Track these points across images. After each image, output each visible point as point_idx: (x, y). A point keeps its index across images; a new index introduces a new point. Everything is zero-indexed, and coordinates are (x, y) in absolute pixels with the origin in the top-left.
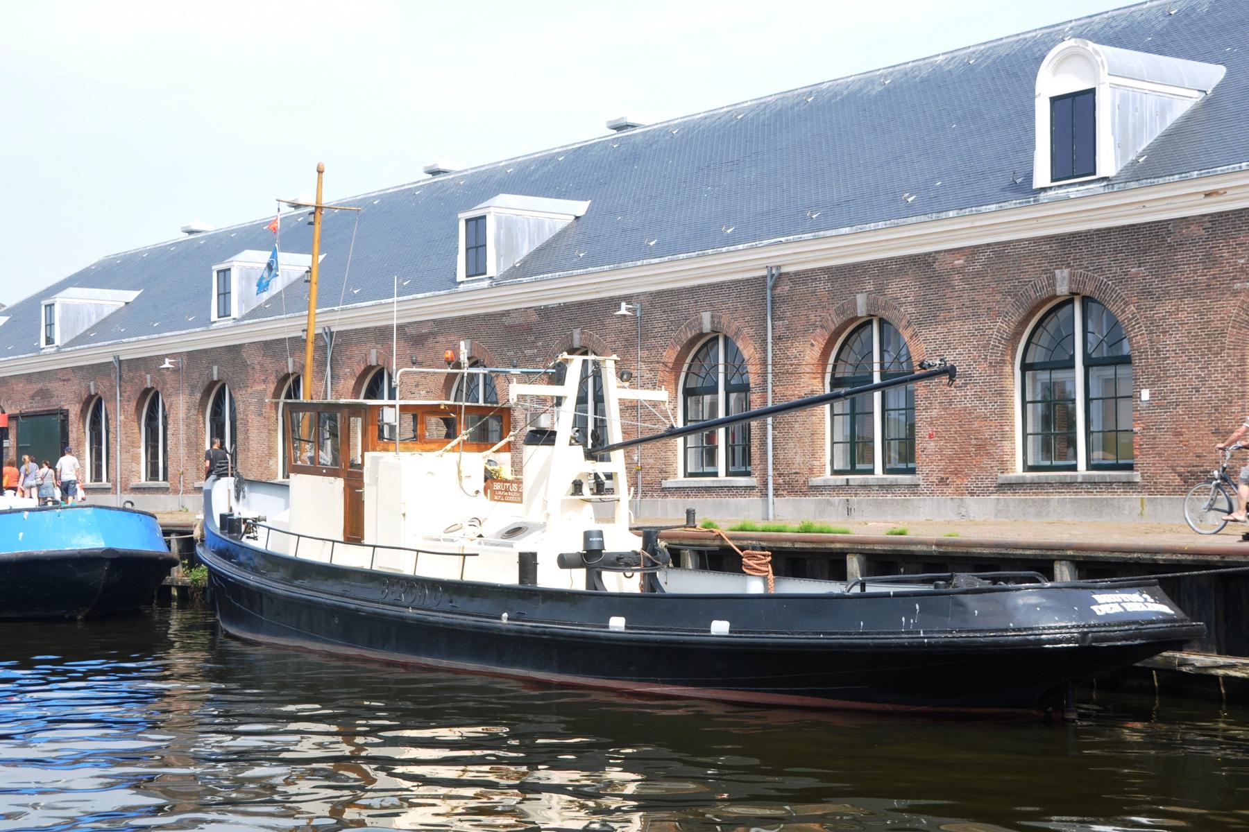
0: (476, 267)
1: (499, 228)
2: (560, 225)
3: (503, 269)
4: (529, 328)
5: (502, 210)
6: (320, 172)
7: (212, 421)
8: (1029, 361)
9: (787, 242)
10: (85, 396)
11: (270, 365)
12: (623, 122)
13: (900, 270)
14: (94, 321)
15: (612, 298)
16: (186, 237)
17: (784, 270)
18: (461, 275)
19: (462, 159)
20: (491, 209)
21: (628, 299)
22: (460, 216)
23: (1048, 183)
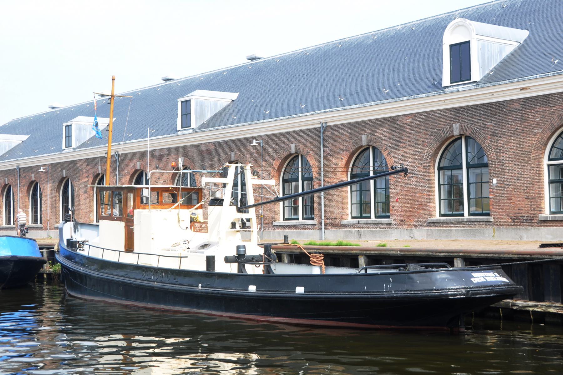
0: (186, 124)
1: (197, 106)
3: (199, 124)
4: (210, 152)
6: (113, 80)
7: (63, 196)
9: (330, 112)
10: (58, 178)
12: (254, 56)
13: (382, 124)
14: (7, 150)
15: (249, 138)
16: (51, 110)
17: (329, 124)
18: (179, 127)
20: (193, 97)
21: (256, 138)
22: (178, 100)
23: (448, 84)
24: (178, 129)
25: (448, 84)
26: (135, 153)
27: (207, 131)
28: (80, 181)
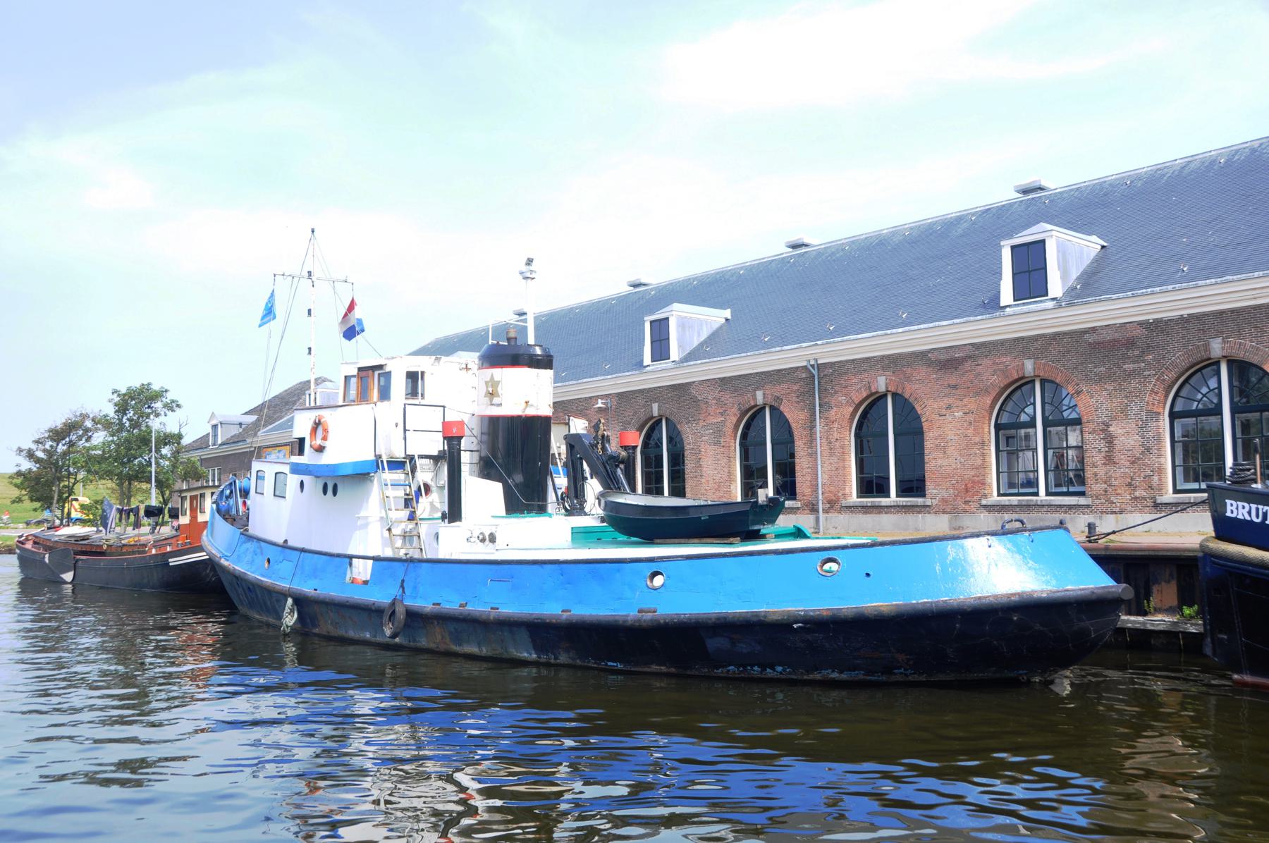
0: (661, 351)
2: (715, 326)
4: (1130, 343)
5: (677, 313)
7: (741, 444)
8: (1177, 409)
9: (1143, 295)
11: (728, 398)
12: (800, 242)
15: (591, 398)
18: (647, 359)
19: (657, 275)
21: (602, 397)
24: (1002, 304)
25: (1011, 302)
26: (1003, 343)
27: (1086, 303)
28: (702, 423)
